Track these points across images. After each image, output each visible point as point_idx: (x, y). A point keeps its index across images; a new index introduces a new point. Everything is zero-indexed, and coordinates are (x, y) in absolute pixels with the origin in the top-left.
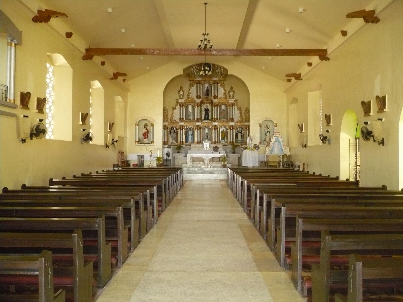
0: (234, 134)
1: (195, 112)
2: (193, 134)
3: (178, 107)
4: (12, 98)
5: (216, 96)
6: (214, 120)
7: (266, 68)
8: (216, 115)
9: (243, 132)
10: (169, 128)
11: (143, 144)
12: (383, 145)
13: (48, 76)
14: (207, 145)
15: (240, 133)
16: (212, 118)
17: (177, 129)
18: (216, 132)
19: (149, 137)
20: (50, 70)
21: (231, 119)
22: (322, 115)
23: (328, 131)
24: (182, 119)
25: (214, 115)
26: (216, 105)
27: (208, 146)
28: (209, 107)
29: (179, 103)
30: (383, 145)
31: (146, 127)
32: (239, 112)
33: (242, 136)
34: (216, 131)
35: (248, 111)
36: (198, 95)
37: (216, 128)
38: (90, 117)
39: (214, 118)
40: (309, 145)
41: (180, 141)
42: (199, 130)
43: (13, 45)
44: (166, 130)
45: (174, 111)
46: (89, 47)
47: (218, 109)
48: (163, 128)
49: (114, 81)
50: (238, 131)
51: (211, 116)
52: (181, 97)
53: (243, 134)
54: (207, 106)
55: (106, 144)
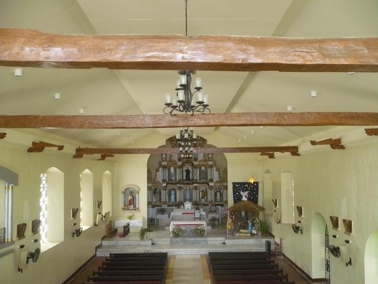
0: (214, 194)
1: (177, 173)
2: (175, 194)
3: (160, 169)
4: (9, 237)
5: (196, 158)
6: (194, 181)
7: (241, 141)
8: (196, 176)
9: (222, 191)
10: (153, 189)
11: (129, 211)
12: (351, 265)
13: (42, 186)
14: (188, 207)
15: (218, 192)
16: (193, 179)
17: (160, 190)
18: (196, 192)
19: (134, 203)
20: (44, 178)
21: (210, 179)
22: (294, 195)
23: (300, 222)
24: (165, 180)
25: (195, 174)
26: (196, 166)
27: (190, 208)
28: (190, 169)
29: (162, 165)
30: (351, 265)
31: (132, 194)
32: (218, 173)
33: (221, 195)
34: (196, 191)
35: (225, 171)
36: (179, 158)
37: (196, 188)
38: (80, 211)
39: (194, 179)
40: (283, 222)
41: (163, 201)
42: (181, 191)
43: (10, 188)
44: (150, 191)
45: (158, 173)
46: (79, 147)
47: (198, 170)
48: (147, 189)
49: (102, 161)
50: (217, 191)
51: (192, 177)
52: (164, 160)
53: (221, 193)
54: (188, 168)
55: (95, 223)
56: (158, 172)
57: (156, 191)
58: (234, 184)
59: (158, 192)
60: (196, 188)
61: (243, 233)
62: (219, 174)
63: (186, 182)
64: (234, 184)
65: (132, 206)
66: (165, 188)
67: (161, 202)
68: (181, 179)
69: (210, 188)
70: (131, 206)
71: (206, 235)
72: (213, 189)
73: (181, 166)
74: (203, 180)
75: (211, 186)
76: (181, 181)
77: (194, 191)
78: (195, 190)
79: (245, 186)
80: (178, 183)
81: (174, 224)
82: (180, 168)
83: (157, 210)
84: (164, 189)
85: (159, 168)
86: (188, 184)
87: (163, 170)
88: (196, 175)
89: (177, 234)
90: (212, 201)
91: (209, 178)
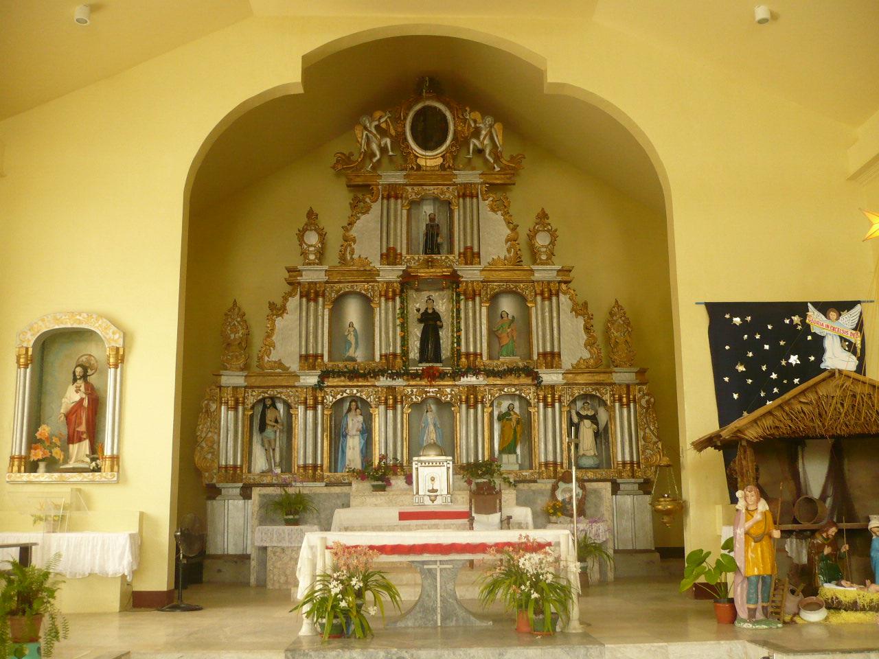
2: (367, 432)
3: (293, 303)
6: (463, 360)
9: (603, 416)
10: (251, 400)
14: (433, 479)
16: (457, 354)
21: (545, 354)
24: (316, 356)
26: (474, 291)
27: (442, 486)
28: (442, 306)
29: (299, 283)
32: (581, 322)
37: (476, 398)
39: (463, 349)
42: (395, 408)
45: (279, 322)
47: (484, 310)
50: (578, 414)
51: (453, 343)
52: (312, 257)
56: (280, 315)
57: (270, 415)
58: (716, 311)
59: (276, 421)
60: (473, 398)
61: (853, 607)
62: (587, 329)
63: (421, 367)
64: (716, 311)
65: (80, 450)
66: (313, 400)
67: (290, 472)
68: (399, 351)
69: (545, 398)
70: (74, 448)
71: (575, 626)
72: (560, 402)
73: (397, 286)
74: (505, 361)
75: (553, 387)
76: (399, 360)
77: (462, 413)
78: (468, 407)
79: (787, 321)
80: (382, 372)
81: (330, 544)
82: (394, 299)
83: (262, 506)
84: (310, 402)
85: (285, 299)
86: (432, 375)
87: (304, 308)
88: (473, 332)
89: (346, 612)
90: (555, 464)
91: (537, 348)
